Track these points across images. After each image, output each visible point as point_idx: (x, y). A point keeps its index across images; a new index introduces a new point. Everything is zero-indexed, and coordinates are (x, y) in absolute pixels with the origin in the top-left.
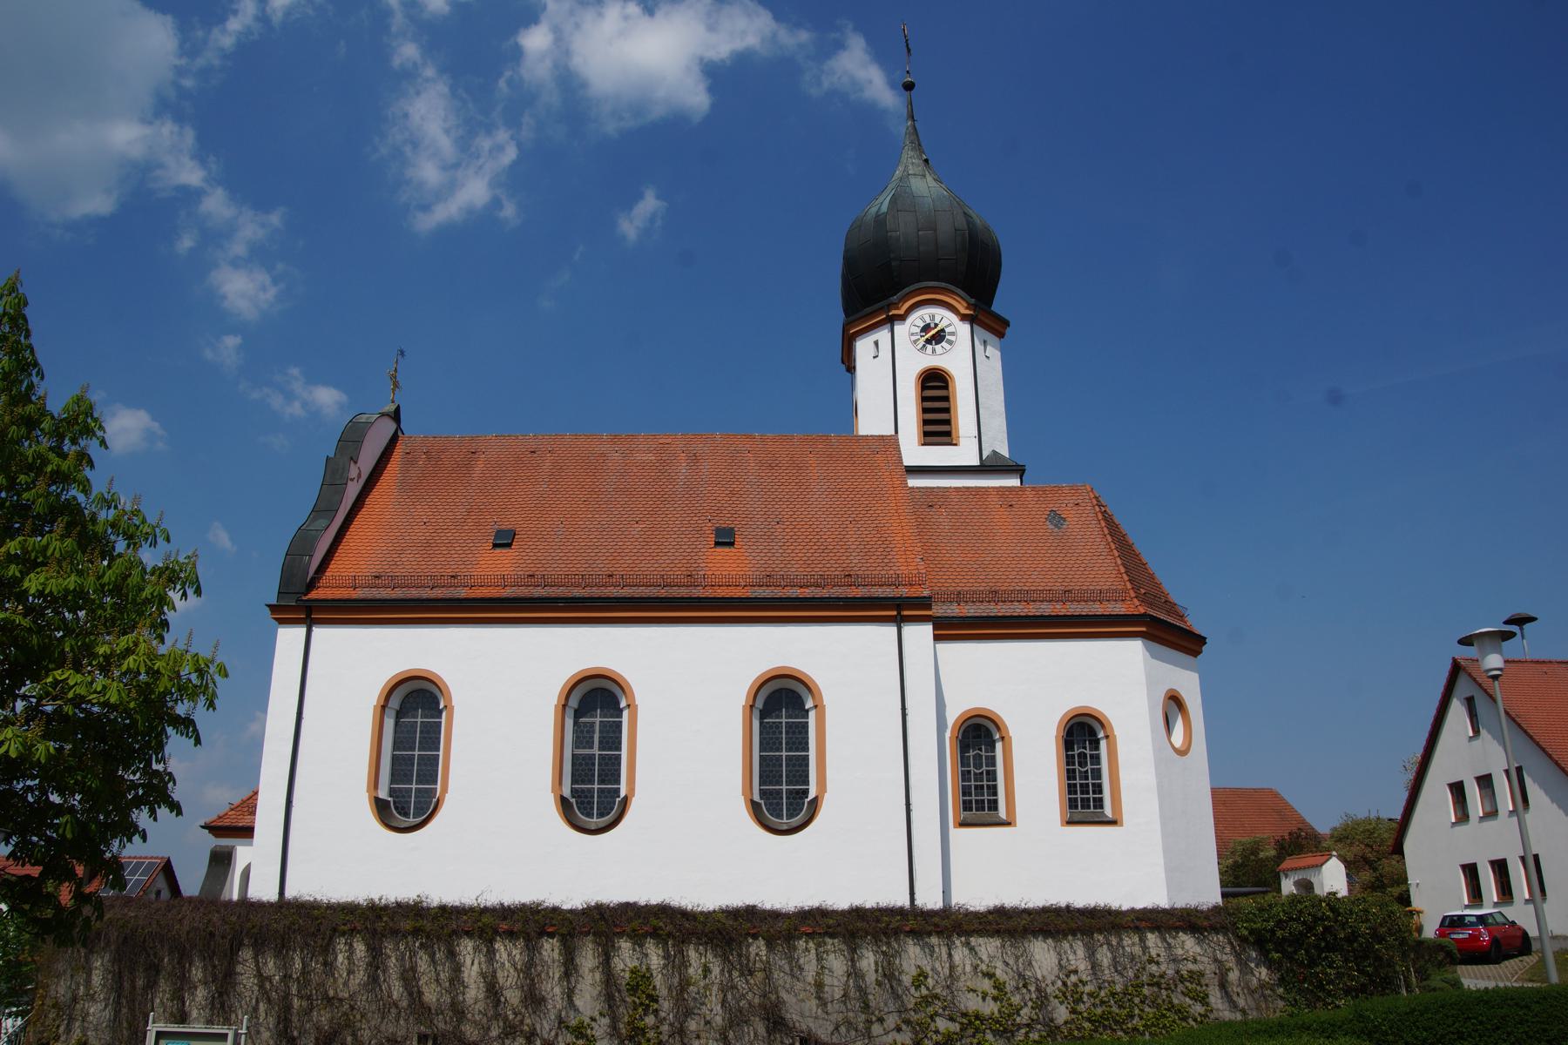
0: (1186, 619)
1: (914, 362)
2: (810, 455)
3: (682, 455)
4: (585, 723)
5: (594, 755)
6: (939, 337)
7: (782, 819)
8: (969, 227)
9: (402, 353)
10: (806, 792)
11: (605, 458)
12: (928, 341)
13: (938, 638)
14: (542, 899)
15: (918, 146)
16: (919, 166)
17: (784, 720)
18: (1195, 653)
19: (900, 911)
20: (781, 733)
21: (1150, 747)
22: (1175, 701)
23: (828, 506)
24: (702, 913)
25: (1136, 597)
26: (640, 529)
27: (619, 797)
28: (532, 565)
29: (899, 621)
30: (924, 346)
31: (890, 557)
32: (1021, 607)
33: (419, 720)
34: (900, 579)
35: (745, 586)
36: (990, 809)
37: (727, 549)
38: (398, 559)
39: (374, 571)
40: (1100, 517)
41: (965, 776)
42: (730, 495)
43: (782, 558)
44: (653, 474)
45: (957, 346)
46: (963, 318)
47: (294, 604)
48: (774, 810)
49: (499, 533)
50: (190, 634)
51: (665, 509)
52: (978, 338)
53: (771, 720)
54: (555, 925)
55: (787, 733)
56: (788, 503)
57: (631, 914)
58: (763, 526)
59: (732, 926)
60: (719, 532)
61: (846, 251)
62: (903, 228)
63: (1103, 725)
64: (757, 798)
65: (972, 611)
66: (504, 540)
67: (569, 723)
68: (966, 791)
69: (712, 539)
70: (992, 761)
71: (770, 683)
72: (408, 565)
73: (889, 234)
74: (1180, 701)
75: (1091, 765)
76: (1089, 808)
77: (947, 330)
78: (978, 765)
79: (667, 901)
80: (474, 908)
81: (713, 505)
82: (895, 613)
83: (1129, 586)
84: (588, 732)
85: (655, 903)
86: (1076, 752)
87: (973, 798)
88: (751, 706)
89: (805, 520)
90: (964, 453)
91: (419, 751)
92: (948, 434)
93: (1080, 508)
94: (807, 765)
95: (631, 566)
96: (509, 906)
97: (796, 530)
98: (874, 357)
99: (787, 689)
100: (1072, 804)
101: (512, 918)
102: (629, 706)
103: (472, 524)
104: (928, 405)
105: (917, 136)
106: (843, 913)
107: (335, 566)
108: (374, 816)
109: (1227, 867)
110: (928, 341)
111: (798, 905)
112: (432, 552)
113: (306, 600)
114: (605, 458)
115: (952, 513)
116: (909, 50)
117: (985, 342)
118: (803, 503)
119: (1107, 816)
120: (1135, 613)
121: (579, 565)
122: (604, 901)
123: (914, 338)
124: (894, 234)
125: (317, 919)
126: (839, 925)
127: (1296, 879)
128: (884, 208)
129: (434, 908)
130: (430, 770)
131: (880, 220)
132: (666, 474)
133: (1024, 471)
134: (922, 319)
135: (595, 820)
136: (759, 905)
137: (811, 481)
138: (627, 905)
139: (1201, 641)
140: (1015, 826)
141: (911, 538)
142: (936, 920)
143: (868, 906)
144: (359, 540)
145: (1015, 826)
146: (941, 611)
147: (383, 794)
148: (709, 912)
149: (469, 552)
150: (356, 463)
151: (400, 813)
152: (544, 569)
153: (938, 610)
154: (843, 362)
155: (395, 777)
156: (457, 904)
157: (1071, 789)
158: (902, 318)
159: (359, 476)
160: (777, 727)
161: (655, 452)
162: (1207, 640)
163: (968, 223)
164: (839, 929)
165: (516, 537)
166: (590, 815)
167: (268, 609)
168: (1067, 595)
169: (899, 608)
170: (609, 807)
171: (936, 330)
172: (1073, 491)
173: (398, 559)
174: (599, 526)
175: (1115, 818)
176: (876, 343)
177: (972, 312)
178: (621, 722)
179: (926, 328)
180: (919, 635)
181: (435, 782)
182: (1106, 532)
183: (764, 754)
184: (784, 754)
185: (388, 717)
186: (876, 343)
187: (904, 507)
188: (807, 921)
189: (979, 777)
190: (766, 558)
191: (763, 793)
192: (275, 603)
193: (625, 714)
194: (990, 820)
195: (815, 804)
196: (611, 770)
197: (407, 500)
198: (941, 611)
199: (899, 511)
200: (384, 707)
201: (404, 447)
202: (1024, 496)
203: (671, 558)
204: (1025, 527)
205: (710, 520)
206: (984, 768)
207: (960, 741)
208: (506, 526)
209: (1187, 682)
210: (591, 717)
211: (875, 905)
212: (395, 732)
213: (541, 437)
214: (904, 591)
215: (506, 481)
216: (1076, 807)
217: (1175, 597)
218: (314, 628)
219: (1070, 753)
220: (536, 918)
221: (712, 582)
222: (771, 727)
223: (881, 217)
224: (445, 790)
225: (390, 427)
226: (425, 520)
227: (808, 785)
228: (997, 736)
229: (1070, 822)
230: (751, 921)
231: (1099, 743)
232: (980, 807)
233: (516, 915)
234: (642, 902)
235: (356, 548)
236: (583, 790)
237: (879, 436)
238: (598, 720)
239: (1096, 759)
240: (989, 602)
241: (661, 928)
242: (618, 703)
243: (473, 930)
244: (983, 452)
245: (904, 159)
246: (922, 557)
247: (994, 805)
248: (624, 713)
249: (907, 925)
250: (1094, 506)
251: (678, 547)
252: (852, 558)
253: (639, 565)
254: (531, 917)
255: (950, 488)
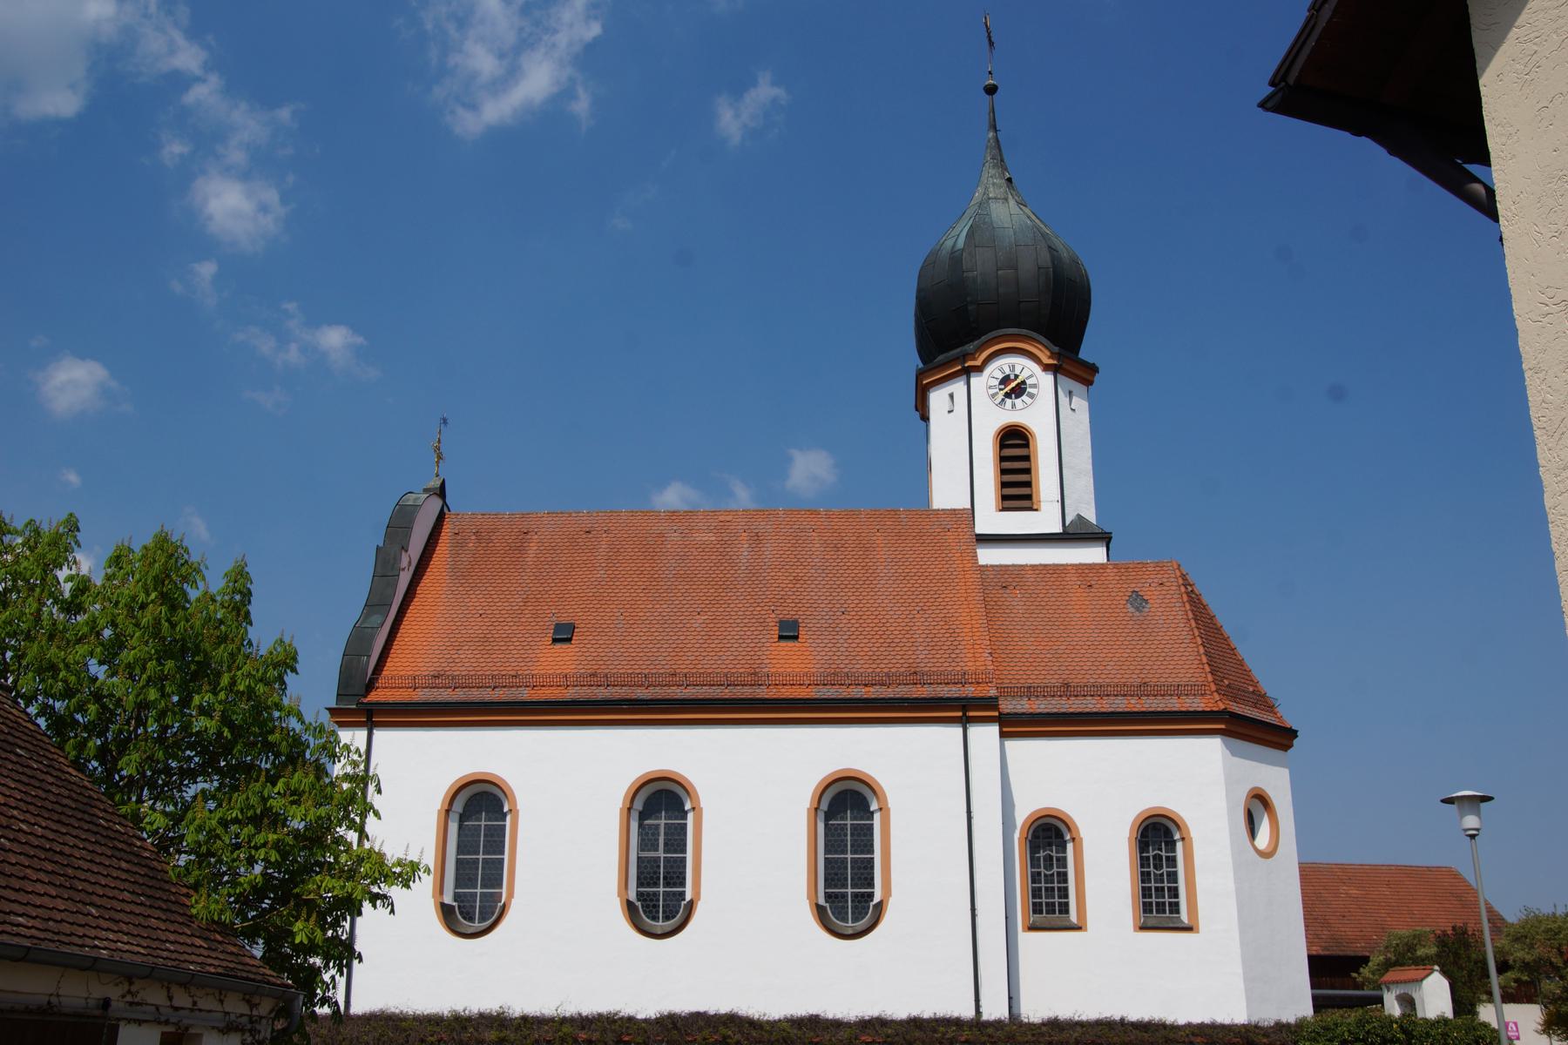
0: (1278, 709)
1: (992, 417)
2: (878, 534)
3: (743, 534)
4: (650, 826)
5: (660, 857)
6: (1019, 390)
7: (847, 923)
8: (1054, 264)
9: (445, 421)
10: (871, 896)
11: (663, 539)
12: (1008, 395)
13: (1004, 735)
14: (618, 1009)
15: (1001, 163)
16: (1001, 187)
17: (849, 822)
18: (1286, 747)
19: (957, 1023)
20: (846, 835)
21: (1228, 852)
22: (1258, 805)
23: (895, 593)
24: (768, 1022)
25: (1216, 691)
26: (702, 621)
27: (684, 900)
28: (594, 662)
29: (965, 722)
30: (1003, 400)
31: (957, 651)
32: (1094, 702)
33: (483, 823)
34: (966, 677)
35: (809, 685)
36: (1060, 912)
37: (790, 644)
38: (456, 656)
39: (431, 671)
40: (1185, 598)
41: (1035, 878)
42: (794, 582)
43: (847, 653)
44: (714, 557)
45: (1039, 401)
46: (1046, 368)
47: (354, 706)
48: (839, 913)
49: (559, 627)
50: (408, 847)
51: (727, 598)
52: (1063, 390)
53: (835, 822)
54: (630, 1034)
55: (852, 835)
56: (854, 590)
57: (701, 1023)
58: (827, 617)
59: (796, 1035)
60: (783, 624)
61: (919, 291)
62: (981, 266)
63: (1178, 827)
64: (822, 901)
65: (1043, 706)
66: (563, 634)
67: (634, 825)
68: (1036, 893)
69: (776, 633)
70: (1063, 862)
71: (834, 785)
72: (467, 663)
73: (965, 274)
74: (1265, 798)
75: (1167, 867)
76: (1165, 913)
77: (1028, 382)
78: (1049, 866)
79: (735, 1010)
80: (554, 1018)
81: (776, 593)
82: (960, 714)
83: (1210, 678)
84: (653, 834)
85: (724, 1012)
86: (1151, 854)
87: (1044, 900)
88: (816, 809)
89: (871, 609)
90: (1046, 519)
91: (483, 854)
92: (1029, 497)
93: (1165, 588)
94: (872, 868)
95: (694, 662)
96: (587, 1017)
97: (861, 621)
98: (950, 412)
99: (851, 790)
100: (1147, 908)
101: (590, 1027)
102: (694, 809)
103: (530, 615)
104: (1008, 465)
105: (1000, 150)
106: (901, 1023)
107: (392, 664)
108: (440, 921)
109: (1378, 965)
110: (1008, 395)
111: (859, 1015)
112: (490, 647)
113: (366, 703)
114: (663, 539)
115: (1026, 595)
116: (991, 44)
117: (1070, 392)
118: (869, 590)
119: (1182, 922)
120: (1215, 709)
121: (641, 662)
122: (677, 1011)
123: (992, 391)
124: (970, 274)
125: (405, 1030)
126: (897, 1035)
127: (1398, 993)
128: (961, 244)
129: (516, 1018)
130: (494, 874)
131: (956, 258)
132: (728, 557)
133: (1110, 539)
134: (1001, 370)
135: (660, 923)
136: (822, 1015)
137: (878, 564)
138: (698, 1014)
139: (1292, 734)
140: (1086, 930)
141: (981, 629)
142: (990, 1031)
143: (926, 1016)
144: (414, 635)
145: (1086, 930)
146: (1010, 707)
147: (448, 899)
148: (775, 1021)
149: (528, 647)
150: (407, 551)
151: (465, 918)
152: (606, 667)
153: (1007, 706)
154: (917, 410)
155: (459, 883)
156: (538, 1014)
157: (1146, 892)
158: (979, 369)
159: (410, 563)
160: (842, 829)
161: (715, 531)
162: (1298, 734)
163: (1053, 258)
164: (897, 1038)
165: (576, 630)
166: (655, 918)
167: (327, 712)
168: (1143, 690)
169: (964, 708)
170: (674, 910)
171: (1016, 383)
172: (1158, 569)
173: (456, 656)
174: (660, 618)
175: (1191, 924)
176: (951, 396)
177: (1055, 362)
178: (686, 824)
179: (1005, 380)
180: (985, 736)
181: (500, 886)
182: (1191, 616)
183: (829, 856)
184: (849, 856)
185: (453, 821)
186: (951, 396)
187: (974, 594)
188: (867, 1030)
189: (1049, 879)
190: (831, 653)
191: (828, 896)
192: (335, 706)
193: (690, 816)
194: (1060, 924)
195: (880, 907)
196: (676, 875)
197: (460, 589)
198: (1010, 707)
199: (969, 591)
200: (448, 811)
201: (452, 527)
202: (1105, 574)
203: (734, 654)
204: (1104, 611)
205: (773, 611)
206: (1055, 869)
207: (1030, 841)
208: (565, 619)
209: (1274, 777)
210: (656, 819)
211: (932, 1016)
212: (459, 835)
213: (595, 515)
214: (970, 691)
215: (562, 566)
216: (1151, 912)
217: (1269, 687)
218: (375, 731)
219: (1144, 855)
220: (613, 1027)
221: (775, 680)
222: (836, 829)
223: (957, 253)
224: (511, 895)
225: (436, 504)
226: (480, 612)
227: (873, 888)
228: (1068, 837)
229: (1143, 928)
230: (815, 1030)
231: (1175, 845)
232: (1051, 910)
233: (594, 1025)
234: (712, 1012)
235: (411, 643)
236: (648, 894)
237: (951, 510)
238: (663, 822)
239: (1172, 861)
240: (1060, 696)
241: (729, 1037)
242: (682, 805)
243: (554, 1039)
244: (1066, 517)
245: (984, 179)
246: (990, 651)
247: (1065, 909)
248: (689, 815)
249: (962, 1036)
250: (1179, 586)
251: (741, 641)
252: (918, 652)
253: (701, 662)
254: (608, 1027)
255: (1027, 565)
